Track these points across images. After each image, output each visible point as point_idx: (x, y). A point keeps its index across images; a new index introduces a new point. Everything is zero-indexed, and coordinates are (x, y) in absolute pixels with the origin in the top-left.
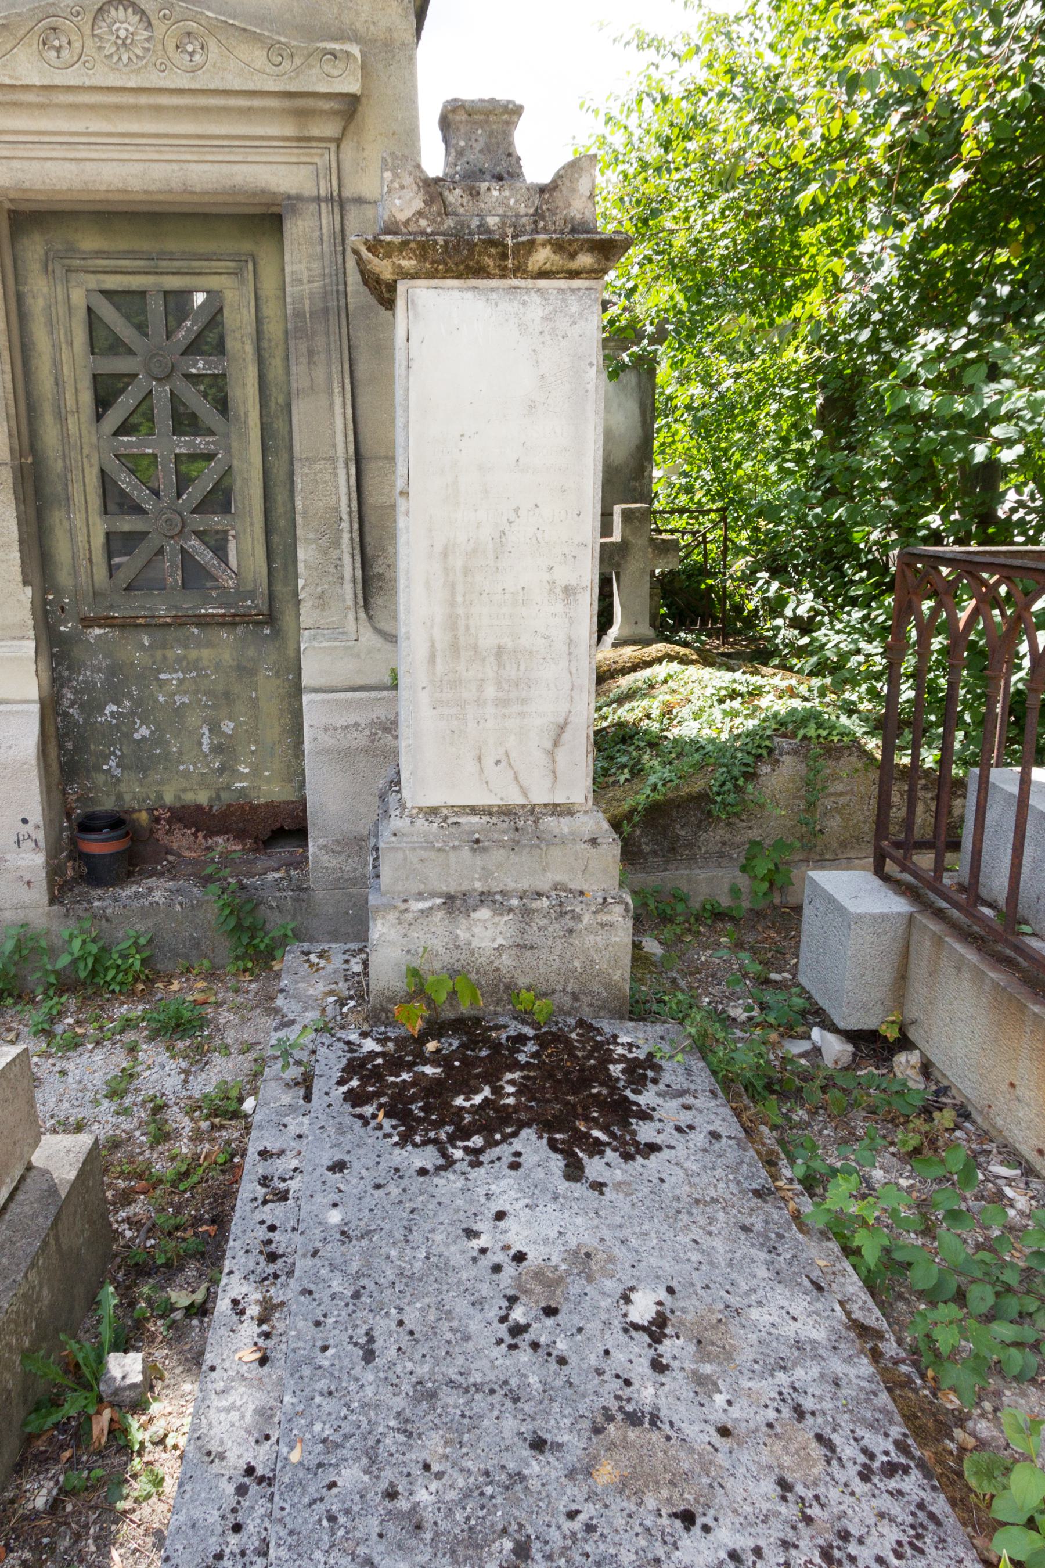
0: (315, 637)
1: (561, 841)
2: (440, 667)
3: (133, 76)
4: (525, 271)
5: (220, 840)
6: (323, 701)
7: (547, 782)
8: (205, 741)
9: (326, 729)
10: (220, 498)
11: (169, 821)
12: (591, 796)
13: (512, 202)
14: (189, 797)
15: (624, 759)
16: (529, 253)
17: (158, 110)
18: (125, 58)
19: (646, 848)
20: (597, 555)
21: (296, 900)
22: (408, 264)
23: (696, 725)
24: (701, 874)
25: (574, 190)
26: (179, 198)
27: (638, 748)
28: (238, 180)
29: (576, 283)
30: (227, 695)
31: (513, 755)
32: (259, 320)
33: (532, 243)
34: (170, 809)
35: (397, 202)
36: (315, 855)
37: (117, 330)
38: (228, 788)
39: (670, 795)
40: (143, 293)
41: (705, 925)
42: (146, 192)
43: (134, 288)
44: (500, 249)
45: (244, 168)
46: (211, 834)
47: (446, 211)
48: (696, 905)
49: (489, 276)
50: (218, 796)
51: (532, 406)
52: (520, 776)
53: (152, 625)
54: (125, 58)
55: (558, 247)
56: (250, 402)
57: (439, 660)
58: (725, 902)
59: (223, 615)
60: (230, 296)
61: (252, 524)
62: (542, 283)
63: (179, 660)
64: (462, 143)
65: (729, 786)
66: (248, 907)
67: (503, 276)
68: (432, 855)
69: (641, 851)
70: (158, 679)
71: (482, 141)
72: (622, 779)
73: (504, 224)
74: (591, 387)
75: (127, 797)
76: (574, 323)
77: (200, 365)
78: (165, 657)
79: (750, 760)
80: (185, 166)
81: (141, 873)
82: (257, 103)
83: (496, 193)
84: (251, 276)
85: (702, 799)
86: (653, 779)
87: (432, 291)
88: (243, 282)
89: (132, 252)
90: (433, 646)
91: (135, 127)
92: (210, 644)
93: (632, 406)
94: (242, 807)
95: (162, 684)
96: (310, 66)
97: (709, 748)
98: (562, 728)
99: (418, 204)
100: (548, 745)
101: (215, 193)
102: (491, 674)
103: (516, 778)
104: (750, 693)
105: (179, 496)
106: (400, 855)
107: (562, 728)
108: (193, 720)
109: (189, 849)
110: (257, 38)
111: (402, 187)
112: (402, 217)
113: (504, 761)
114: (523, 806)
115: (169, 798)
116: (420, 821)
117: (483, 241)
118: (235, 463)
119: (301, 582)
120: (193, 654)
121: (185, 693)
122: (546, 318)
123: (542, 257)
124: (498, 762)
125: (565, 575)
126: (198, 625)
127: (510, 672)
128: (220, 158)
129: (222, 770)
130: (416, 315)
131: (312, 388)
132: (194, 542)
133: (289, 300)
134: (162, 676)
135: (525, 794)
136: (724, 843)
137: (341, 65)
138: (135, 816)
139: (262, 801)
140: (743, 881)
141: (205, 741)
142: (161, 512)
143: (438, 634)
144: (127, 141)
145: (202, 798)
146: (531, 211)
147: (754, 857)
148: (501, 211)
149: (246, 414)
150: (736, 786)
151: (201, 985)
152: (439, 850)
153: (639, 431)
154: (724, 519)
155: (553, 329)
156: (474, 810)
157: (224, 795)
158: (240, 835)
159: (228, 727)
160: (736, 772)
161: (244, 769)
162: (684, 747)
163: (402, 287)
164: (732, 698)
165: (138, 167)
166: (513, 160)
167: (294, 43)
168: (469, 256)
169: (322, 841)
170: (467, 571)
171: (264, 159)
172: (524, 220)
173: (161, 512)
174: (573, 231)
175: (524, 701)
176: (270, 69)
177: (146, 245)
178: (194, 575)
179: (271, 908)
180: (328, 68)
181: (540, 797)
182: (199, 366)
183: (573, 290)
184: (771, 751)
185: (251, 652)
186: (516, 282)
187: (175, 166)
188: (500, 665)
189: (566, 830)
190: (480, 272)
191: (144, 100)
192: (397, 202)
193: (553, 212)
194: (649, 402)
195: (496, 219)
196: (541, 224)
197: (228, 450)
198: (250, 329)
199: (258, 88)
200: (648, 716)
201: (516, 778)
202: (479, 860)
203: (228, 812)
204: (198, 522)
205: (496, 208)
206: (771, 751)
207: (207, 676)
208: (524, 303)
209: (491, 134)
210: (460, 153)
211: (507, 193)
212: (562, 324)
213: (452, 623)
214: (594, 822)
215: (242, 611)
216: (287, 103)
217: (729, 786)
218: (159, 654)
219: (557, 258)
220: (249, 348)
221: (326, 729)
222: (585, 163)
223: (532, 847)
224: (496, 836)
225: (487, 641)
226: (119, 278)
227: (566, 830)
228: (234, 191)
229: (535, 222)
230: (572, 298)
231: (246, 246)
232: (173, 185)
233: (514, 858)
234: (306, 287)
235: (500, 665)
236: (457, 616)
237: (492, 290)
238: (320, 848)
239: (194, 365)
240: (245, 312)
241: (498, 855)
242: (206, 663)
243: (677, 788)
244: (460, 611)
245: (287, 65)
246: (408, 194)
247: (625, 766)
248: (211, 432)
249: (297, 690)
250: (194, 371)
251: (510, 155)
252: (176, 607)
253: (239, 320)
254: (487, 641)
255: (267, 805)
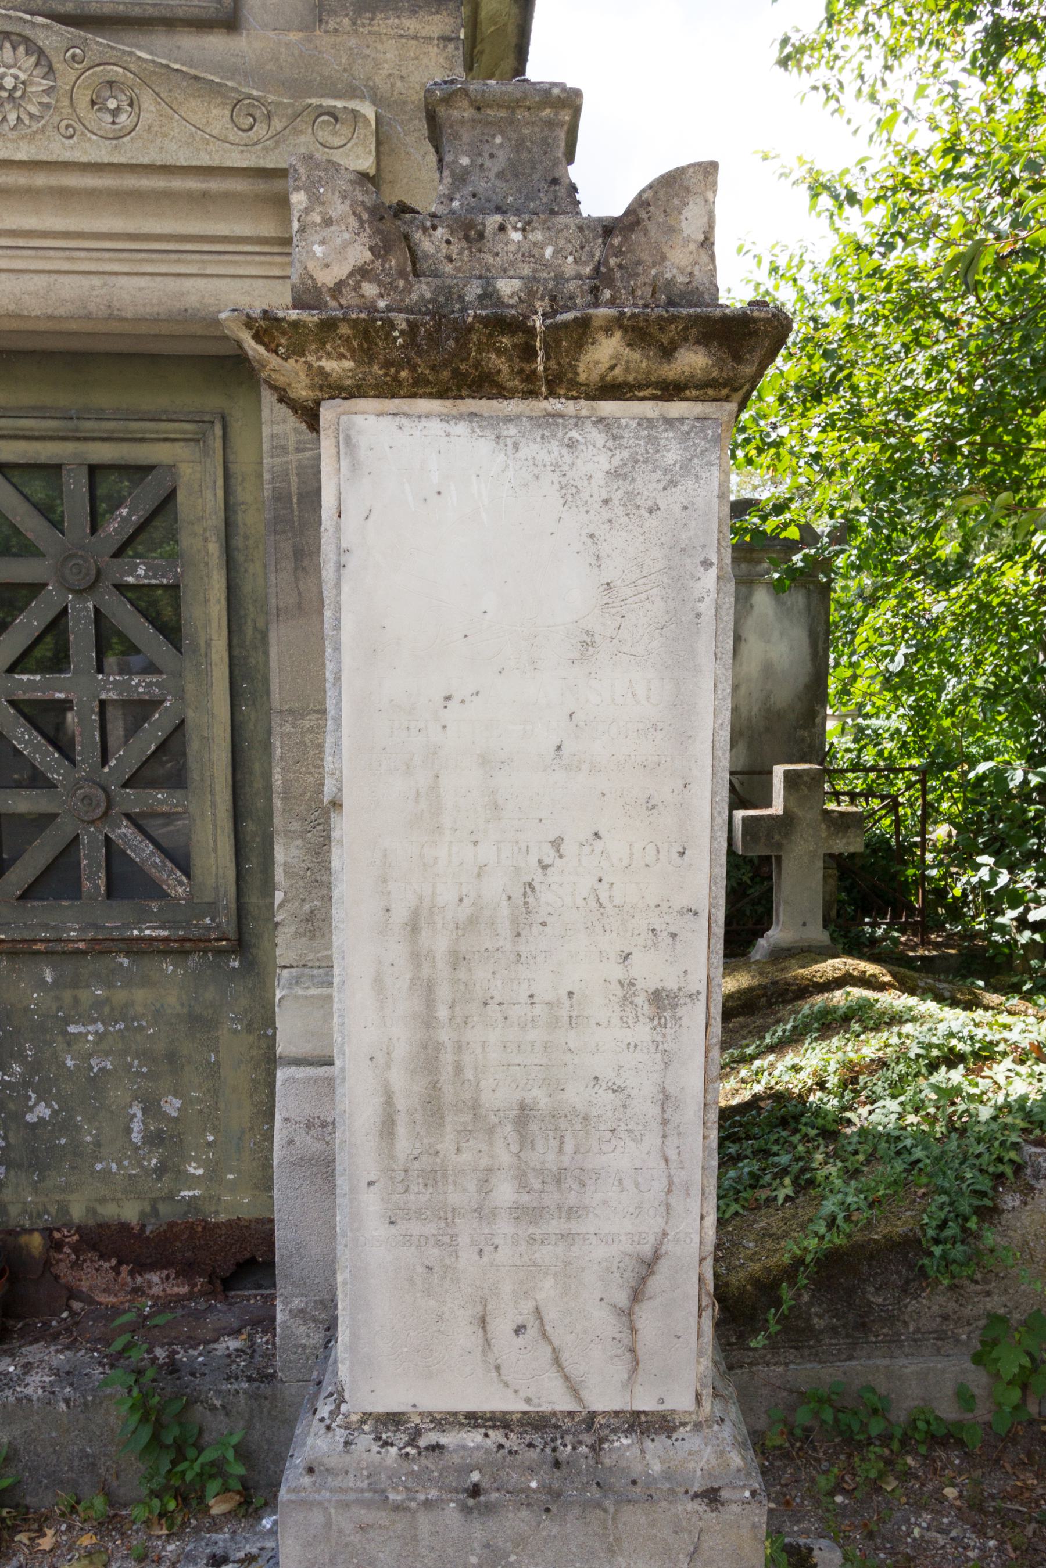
0: (297, 981)
1: (642, 1492)
2: (403, 1145)
3: (23, 145)
4: (573, 384)
5: (155, 1277)
6: (308, 1079)
7: (619, 1371)
8: (136, 1126)
9: (309, 1126)
10: (168, 764)
11: (76, 1249)
12: (707, 1393)
13: (549, 252)
14: (109, 1212)
15: (784, 1159)
16: (579, 346)
17: (64, 194)
18: (12, 117)
19: (818, 1323)
20: (720, 930)
21: (254, 1396)
22: (338, 367)
23: (893, 1105)
24: (909, 1366)
25: (672, 230)
26: (101, 328)
27: (806, 1139)
28: (192, 301)
29: (677, 408)
30: (172, 1057)
31: (550, 1315)
32: (229, 507)
33: (584, 324)
34: (79, 1229)
35: (318, 250)
36: (285, 1325)
37: (17, 521)
38: (170, 1198)
39: (858, 1238)
40: (58, 467)
41: (916, 1454)
42: (50, 318)
43: (43, 459)
44: (520, 338)
45: (201, 283)
46: (141, 1267)
47: (416, 265)
48: (900, 1415)
49: (501, 393)
50: (155, 1211)
51: (588, 643)
52: (565, 1356)
53: (58, 952)
54: (12, 117)
55: (638, 332)
56: (215, 624)
57: (401, 1130)
58: (948, 1411)
59: (166, 940)
60: (187, 473)
61: (214, 805)
62: (608, 408)
63: (98, 1004)
64: (465, 161)
65: (953, 1229)
66: (176, 1407)
67: (531, 394)
68: (381, 1517)
69: (810, 1328)
70: (65, 1033)
71: (502, 156)
72: (781, 1194)
73: (531, 293)
74: (707, 608)
75: (14, 1210)
76: (673, 483)
77: (141, 571)
78: (76, 1000)
79: (985, 1184)
80: (113, 280)
81: (23, 1334)
82: (215, 185)
83: (516, 236)
84: (218, 444)
85: (908, 1246)
86: (829, 1206)
87: (386, 421)
88: (206, 453)
89: (42, 408)
90: (389, 1101)
91: (31, 222)
92: (146, 982)
93: (799, 634)
94: (191, 1226)
95: (71, 1040)
96: (298, 132)
97: (918, 1153)
98: (649, 1265)
99: (360, 254)
100: (622, 1298)
101: (156, 320)
102: (505, 1159)
103: (557, 1361)
104: (975, 1054)
105: (104, 762)
106: (317, 1517)
107: (649, 1265)
108: (117, 1094)
109: (106, 1291)
110: (215, 90)
111: (328, 222)
112: (327, 278)
113: (534, 1326)
114: (571, 1414)
115: (77, 1212)
116: (365, 1441)
117: (485, 321)
118: (190, 714)
119: (279, 896)
120: (120, 996)
121: (107, 1054)
122: (615, 474)
123: (606, 353)
124: (520, 1329)
125: (652, 970)
126: (128, 953)
127: (544, 1155)
128: (164, 269)
129: (161, 1170)
130: (355, 466)
131: (299, 606)
132: (126, 830)
133: (267, 476)
134: (72, 1029)
135: (574, 1390)
136: (945, 1318)
137: (344, 130)
138: (23, 1239)
139: (223, 1217)
140: (977, 1380)
141: (136, 1126)
142: (77, 785)
143: (398, 1079)
144: (21, 243)
145: (130, 1212)
146: (587, 270)
147: (995, 1342)
148: (526, 270)
149: (208, 645)
150: (964, 1230)
151: (87, 1540)
152: (397, 1508)
153: (809, 666)
154: (923, 782)
155: (631, 495)
156: (473, 1420)
157: (162, 1209)
158: (187, 1270)
159: (172, 1106)
160: (964, 1206)
161: (195, 1170)
162: (881, 1145)
163: (327, 413)
164: (951, 1065)
165: (39, 282)
166: (562, 191)
167: (271, 98)
168: (464, 353)
169: (297, 1303)
170: (457, 960)
171: (231, 271)
172: (572, 286)
173: (77, 785)
174: (671, 303)
175: (572, 1213)
176: (235, 135)
177: (66, 399)
178: (124, 881)
179: (213, 1408)
180: (323, 135)
181: (605, 1397)
182: (139, 574)
183: (670, 422)
184: (1018, 1168)
185: (210, 994)
186: (555, 405)
187: (96, 281)
188: (525, 1141)
189: (656, 1467)
190: (482, 385)
191: (40, 180)
192: (318, 250)
193: (630, 271)
194: (821, 629)
195: (517, 284)
196: (607, 294)
197: (180, 696)
198: (216, 520)
199: (216, 163)
200: (821, 1085)
201: (557, 1361)
202: (478, 1531)
203: (169, 1234)
204: (132, 799)
205: (518, 264)
206: (1018, 1168)
207: (141, 1028)
208: (572, 445)
209: (520, 146)
210: (461, 178)
211: (538, 236)
212: (647, 485)
213: (428, 1059)
214: (713, 1450)
215: (195, 933)
216: (261, 186)
217: (953, 1229)
218: (67, 995)
219: (636, 356)
220: (214, 548)
221: (309, 1126)
222: (693, 180)
223: (587, 1505)
224: (514, 1478)
225: (499, 1095)
226: (21, 446)
227: (656, 1467)
228: (185, 316)
229: (595, 290)
230: (667, 436)
231: (213, 401)
232: (92, 307)
233: (550, 1527)
234: (293, 457)
235: (525, 1141)
236: (438, 1047)
237: (509, 419)
238: (294, 1314)
239: (132, 572)
240: (209, 494)
241: (517, 1521)
242: (140, 1009)
243: (869, 1225)
244: (445, 1036)
245: (260, 130)
246: (341, 235)
247: (785, 1172)
248: (151, 669)
249: (270, 1061)
250: (131, 580)
251: (555, 181)
252: (95, 926)
253: (200, 503)
254: (499, 1095)
255: (229, 1224)
